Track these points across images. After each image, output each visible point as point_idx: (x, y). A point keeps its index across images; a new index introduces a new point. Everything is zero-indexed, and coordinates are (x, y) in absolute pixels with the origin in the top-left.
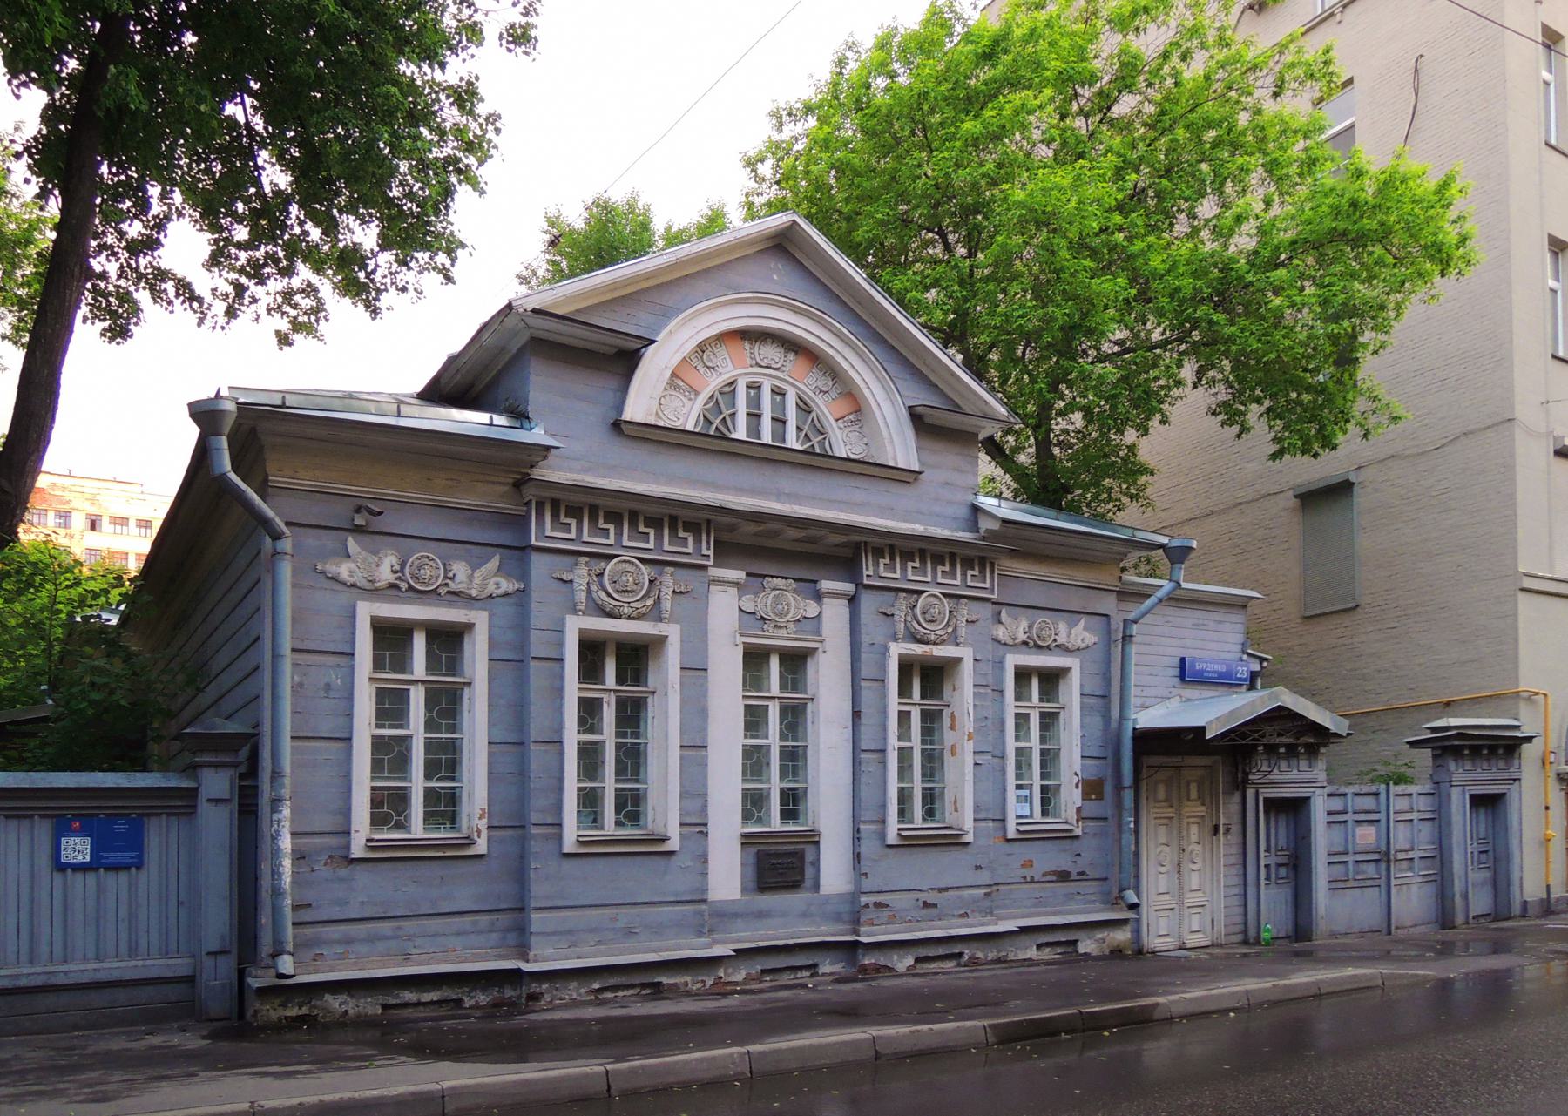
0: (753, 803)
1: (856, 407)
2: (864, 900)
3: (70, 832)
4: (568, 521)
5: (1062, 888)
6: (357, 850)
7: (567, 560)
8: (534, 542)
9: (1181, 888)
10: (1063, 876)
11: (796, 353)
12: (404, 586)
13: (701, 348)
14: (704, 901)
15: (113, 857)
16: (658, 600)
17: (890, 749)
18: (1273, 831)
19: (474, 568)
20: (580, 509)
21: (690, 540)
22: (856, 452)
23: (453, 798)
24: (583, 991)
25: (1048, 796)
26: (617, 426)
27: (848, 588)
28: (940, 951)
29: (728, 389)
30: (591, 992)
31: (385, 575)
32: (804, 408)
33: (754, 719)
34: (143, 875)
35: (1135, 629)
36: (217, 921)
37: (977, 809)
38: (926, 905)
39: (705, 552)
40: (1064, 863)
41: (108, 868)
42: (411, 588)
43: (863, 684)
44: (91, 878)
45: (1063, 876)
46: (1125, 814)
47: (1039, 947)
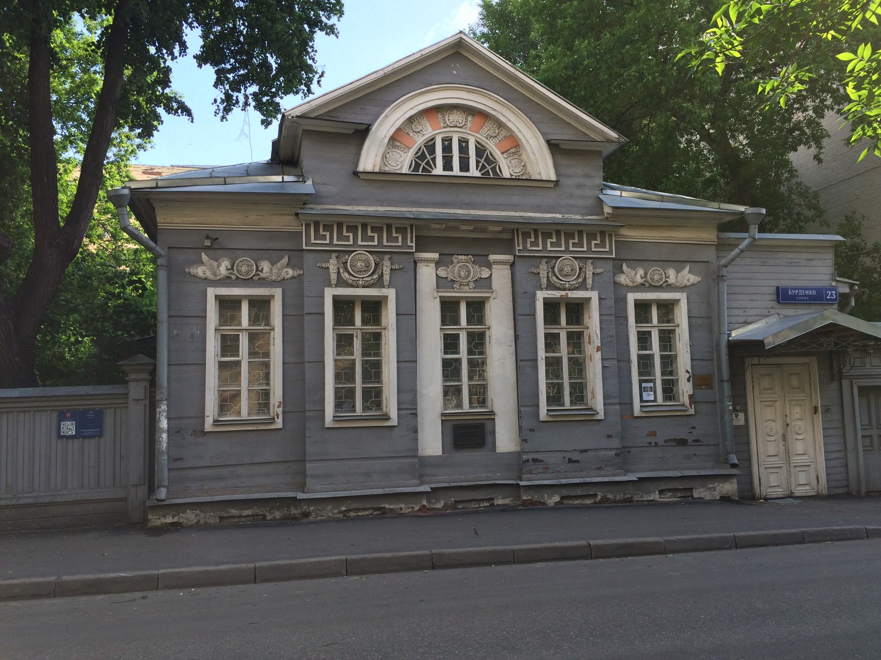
0: (451, 392)
1: (514, 146)
2: (525, 457)
3: (66, 419)
4: (324, 233)
5: (681, 451)
6: (208, 426)
7: (538, 260)
8: (304, 247)
9: (787, 452)
10: (682, 442)
11: (474, 115)
12: (233, 277)
13: (411, 120)
14: (415, 456)
15: (87, 432)
16: (585, 280)
17: (539, 358)
18: (873, 410)
19: (273, 264)
20: (332, 226)
21: (400, 238)
22: (517, 171)
23: (379, 392)
24: (336, 511)
25: (670, 389)
26: (356, 174)
27: (510, 258)
28: (579, 492)
29: (431, 143)
30: (340, 512)
31: (223, 271)
32: (481, 151)
33: (450, 343)
34: (102, 440)
35: (724, 271)
36: (136, 468)
37: (606, 397)
38: (570, 461)
39: (409, 244)
40: (682, 434)
41: (84, 437)
42: (650, 285)
43: (520, 317)
44: (77, 443)
45: (682, 442)
46: (726, 399)
47: (661, 492)
